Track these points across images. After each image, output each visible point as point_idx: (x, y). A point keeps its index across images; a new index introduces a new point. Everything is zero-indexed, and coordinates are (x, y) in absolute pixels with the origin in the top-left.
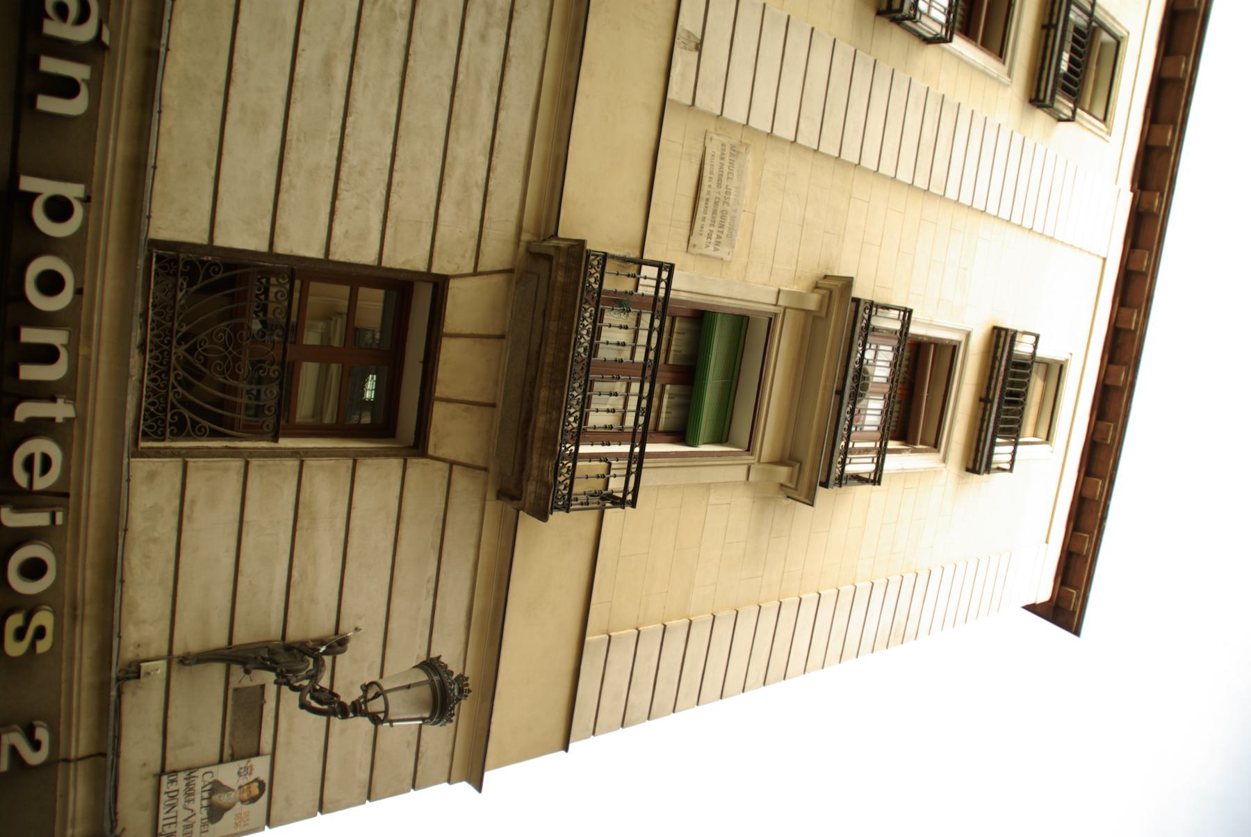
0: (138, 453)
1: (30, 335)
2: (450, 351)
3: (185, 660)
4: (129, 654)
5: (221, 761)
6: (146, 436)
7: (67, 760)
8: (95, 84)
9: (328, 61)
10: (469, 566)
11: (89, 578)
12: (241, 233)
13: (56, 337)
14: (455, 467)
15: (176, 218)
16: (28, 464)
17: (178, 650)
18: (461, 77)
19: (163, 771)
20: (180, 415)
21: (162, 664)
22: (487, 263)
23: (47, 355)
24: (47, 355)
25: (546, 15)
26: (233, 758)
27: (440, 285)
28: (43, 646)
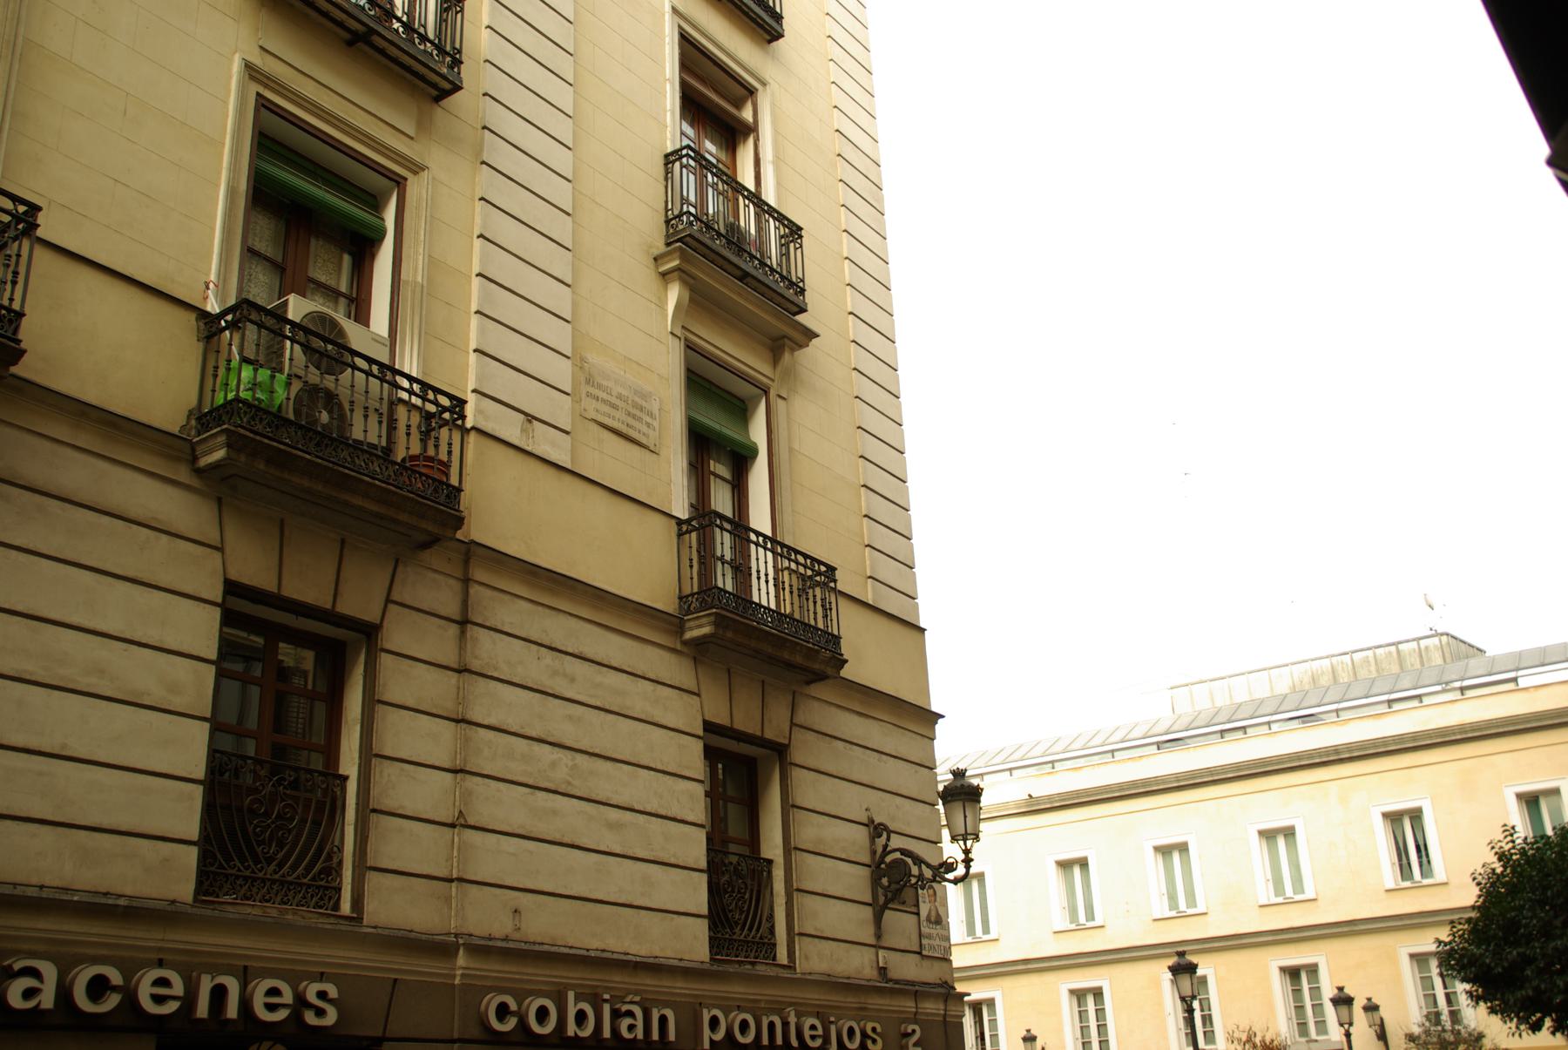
0: (791, 967)
1: (202, 1009)
2: (295, 589)
3: (878, 936)
4: (874, 974)
5: (918, 914)
6: (337, 907)
7: (945, 1016)
8: (215, 970)
9: (613, 826)
10: (839, 712)
11: (851, 1000)
12: (183, 813)
13: (206, 985)
14: (395, 596)
15: (174, 875)
16: (271, 1008)
17: (872, 941)
18: (598, 704)
19: (919, 953)
20: (320, 873)
21: (881, 953)
22: (213, 536)
23: (219, 993)
24: (219, 993)
25: (547, 611)
26: (917, 905)
27: (709, 726)
28: (333, 992)
